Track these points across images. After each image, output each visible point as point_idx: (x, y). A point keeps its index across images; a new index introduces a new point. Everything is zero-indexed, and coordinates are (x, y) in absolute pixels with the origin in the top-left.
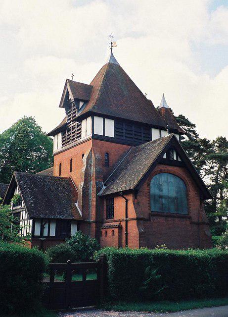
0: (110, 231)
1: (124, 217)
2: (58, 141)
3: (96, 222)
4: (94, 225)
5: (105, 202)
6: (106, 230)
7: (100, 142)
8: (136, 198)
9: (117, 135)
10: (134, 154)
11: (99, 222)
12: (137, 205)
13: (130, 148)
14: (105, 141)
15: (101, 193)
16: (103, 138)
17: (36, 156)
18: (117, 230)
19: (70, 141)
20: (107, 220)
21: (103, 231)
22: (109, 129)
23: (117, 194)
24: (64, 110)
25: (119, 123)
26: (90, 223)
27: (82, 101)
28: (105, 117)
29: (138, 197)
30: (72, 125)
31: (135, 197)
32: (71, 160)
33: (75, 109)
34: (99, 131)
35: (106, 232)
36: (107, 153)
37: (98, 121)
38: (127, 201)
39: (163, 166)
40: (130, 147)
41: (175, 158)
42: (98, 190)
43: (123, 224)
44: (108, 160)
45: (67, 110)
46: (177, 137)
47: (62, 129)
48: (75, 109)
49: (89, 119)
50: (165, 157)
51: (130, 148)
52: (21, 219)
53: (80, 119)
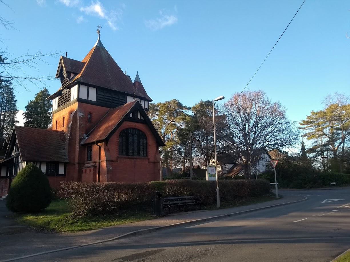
0: (88, 169)
1: (97, 160)
2: (55, 102)
3: (79, 163)
4: (77, 165)
5: (86, 149)
6: (86, 169)
7: (84, 105)
8: (107, 145)
9: (125, 100)
10: (111, 113)
11: (81, 164)
12: (107, 151)
13: (109, 110)
14: (89, 104)
15: (82, 143)
16: (87, 102)
17: (162, 110)
18: (92, 169)
19: (63, 103)
20: (88, 162)
21: (84, 170)
22: (93, 95)
23: (94, 143)
24: (59, 80)
25: (100, 89)
26: (74, 164)
27: (73, 73)
28: (88, 85)
29: (108, 145)
30: (65, 91)
31: (106, 144)
32: (64, 117)
33: (67, 79)
34: (84, 96)
35: (86, 170)
36: (90, 113)
37: (84, 89)
38: (100, 148)
39: (129, 122)
40: (109, 109)
41: (139, 117)
42: (81, 140)
43: (97, 164)
44: (91, 118)
45: (61, 80)
46: (142, 103)
47: (59, 94)
48: (67, 79)
49: (76, 87)
50: (131, 116)
51: (109, 110)
52: (19, 161)
53: (70, 87)
